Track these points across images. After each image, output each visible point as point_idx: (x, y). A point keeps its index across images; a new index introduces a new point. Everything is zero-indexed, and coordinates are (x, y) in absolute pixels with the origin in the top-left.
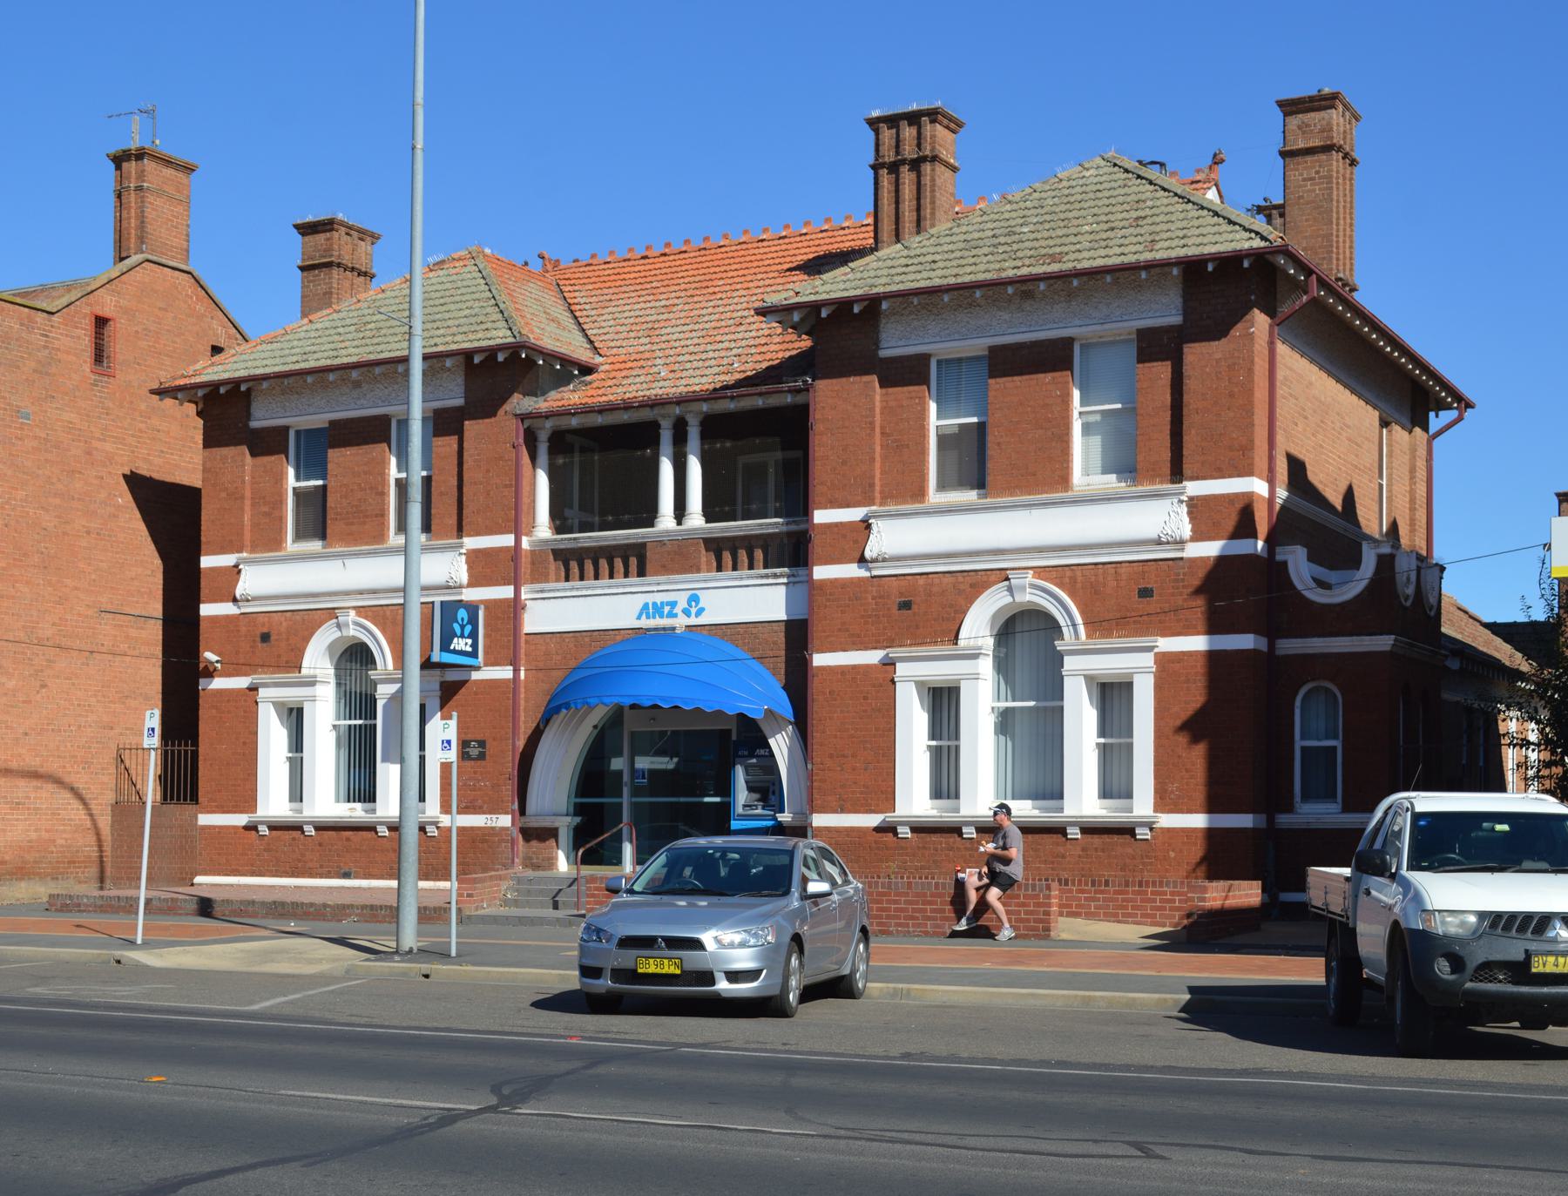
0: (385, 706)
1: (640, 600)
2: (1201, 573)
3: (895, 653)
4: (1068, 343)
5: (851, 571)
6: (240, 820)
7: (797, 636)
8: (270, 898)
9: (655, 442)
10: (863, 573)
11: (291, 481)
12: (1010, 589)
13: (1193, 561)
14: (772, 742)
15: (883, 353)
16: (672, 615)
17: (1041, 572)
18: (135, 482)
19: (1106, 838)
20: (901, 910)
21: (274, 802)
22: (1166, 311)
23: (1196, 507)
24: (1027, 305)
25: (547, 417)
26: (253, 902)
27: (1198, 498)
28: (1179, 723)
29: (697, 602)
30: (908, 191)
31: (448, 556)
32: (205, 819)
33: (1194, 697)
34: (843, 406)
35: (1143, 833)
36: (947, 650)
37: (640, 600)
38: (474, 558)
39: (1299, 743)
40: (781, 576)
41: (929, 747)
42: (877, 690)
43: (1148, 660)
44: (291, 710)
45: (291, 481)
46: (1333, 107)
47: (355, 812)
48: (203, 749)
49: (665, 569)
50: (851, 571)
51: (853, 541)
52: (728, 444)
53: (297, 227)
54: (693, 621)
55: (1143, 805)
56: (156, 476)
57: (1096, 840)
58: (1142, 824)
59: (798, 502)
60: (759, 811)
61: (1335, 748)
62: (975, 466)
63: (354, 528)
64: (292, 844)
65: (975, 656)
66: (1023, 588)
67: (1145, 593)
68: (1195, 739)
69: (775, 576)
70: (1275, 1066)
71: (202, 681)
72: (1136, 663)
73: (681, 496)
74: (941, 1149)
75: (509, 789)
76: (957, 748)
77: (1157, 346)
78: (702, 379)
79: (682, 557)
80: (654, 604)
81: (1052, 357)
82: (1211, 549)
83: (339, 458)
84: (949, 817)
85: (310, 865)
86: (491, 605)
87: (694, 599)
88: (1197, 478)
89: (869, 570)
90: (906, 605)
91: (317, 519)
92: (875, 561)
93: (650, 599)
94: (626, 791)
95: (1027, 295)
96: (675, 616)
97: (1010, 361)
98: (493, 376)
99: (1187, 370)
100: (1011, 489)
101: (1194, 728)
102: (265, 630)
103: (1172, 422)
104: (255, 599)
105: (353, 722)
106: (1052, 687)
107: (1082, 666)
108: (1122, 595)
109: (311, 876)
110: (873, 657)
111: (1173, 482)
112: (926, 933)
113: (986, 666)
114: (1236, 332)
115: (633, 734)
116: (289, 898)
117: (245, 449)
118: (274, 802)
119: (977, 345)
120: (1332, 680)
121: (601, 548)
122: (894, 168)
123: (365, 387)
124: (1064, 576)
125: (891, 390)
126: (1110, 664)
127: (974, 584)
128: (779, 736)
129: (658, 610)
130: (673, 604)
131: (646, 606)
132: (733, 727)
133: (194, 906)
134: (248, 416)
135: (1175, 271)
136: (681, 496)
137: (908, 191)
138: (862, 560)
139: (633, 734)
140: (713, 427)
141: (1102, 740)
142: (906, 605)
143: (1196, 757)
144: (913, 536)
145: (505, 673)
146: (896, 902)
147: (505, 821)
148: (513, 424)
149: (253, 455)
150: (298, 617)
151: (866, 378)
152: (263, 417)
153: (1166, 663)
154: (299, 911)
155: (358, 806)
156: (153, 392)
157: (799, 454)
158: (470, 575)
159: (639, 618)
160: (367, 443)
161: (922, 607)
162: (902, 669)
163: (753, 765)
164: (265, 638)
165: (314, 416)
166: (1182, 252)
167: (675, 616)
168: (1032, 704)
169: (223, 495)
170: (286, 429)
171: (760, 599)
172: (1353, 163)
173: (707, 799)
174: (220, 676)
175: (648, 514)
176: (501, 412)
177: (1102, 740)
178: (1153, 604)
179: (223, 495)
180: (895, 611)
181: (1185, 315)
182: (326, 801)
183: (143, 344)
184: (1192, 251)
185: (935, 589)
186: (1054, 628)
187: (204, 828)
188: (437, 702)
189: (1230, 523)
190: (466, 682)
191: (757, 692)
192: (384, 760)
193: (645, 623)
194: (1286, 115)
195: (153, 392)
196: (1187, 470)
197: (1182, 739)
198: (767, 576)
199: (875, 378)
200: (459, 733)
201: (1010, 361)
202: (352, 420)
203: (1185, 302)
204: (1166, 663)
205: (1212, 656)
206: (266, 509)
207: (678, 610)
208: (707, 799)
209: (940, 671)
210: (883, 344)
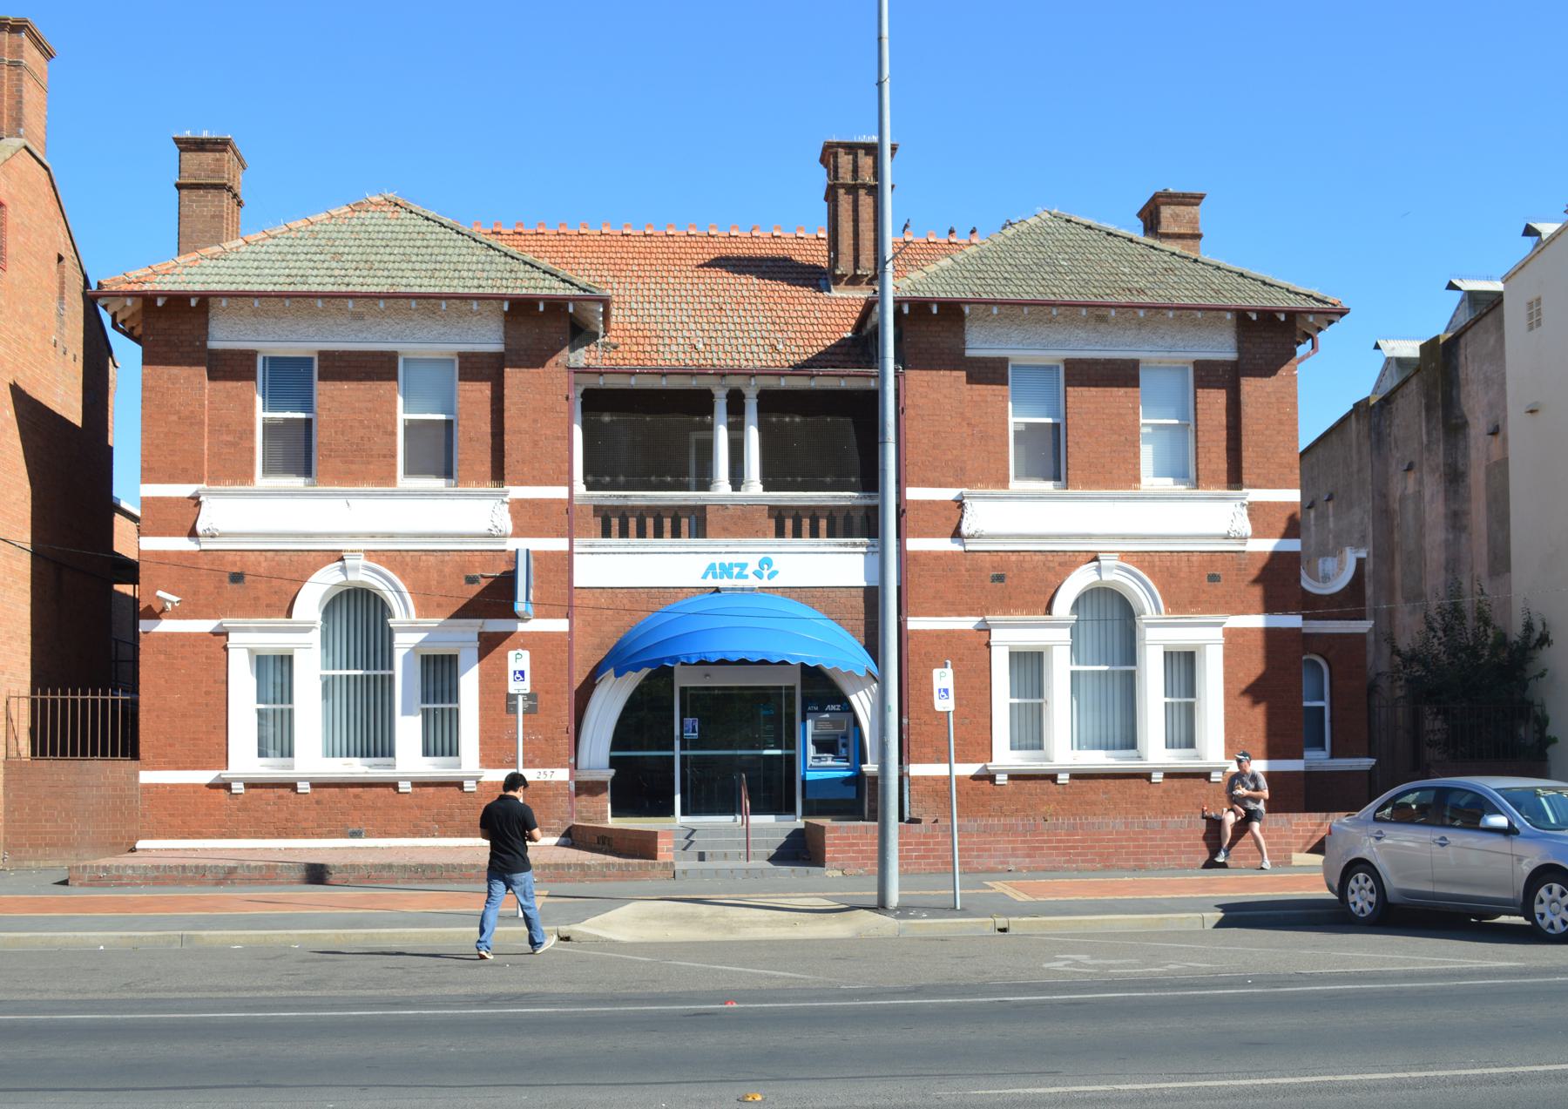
0: (405, 657)
1: (707, 560)
2: (1260, 564)
3: (228, 622)
4: (1004, 362)
5: (945, 545)
6: (205, 777)
7: (872, 597)
8: (405, 861)
9: (709, 410)
10: (956, 547)
11: (261, 414)
12: (1099, 569)
13: (1252, 554)
14: (853, 699)
15: (969, 353)
16: (741, 576)
18: (16, 391)
19: (1191, 781)
20: (1158, 846)
21: (245, 759)
22: (1222, 348)
23: (1254, 510)
24: (1102, 327)
25: (752, 375)
26: (390, 867)
27: (1256, 503)
28: (1243, 687)
29: (770, 564)
30: (866, 212)
31: (488, 504)
32: (147, 777)
33: (1255, 666)
34: (910, 398)
36: (281, 621)
37: (707, 560)
39: (1325, 704)
40: (861, 545)
42: (971, 657)
43: (1218, 633)
44: (259, 657)
45: (261, 414)
46: (225, 150)
47: (357, 768)
49: (726, 532)
50: (945, 545)
51: (951, 520)
52: (797, 419)
53: (177, 141)
54: (765, 583)
55: (1212, 751)
57: (1177, 783)
58: (1217, 769)
59: (870, 480)
60: (829, 763)
62: (1052, 458)
63: (354, 467)
64: (273, 804)
65: (307, 630)
66: (356, 569)
67: (1213, 578)
68: (1256, 702)
69: (855, 545)
70: (1476, 964)
71: (144, 625)
72: (1207, 637)
73: (737, 468)
75: (565, 743)
76: (291, 712)
77: (1206, 375)
78: (760, 358)
79: (740, 522)
80: (722, 565)
81: (1123, 375)
82: (1268, 545)
83: (330, 395)
84: (1045, 767)
85: (304, 825)
86: (542, 558)
87: (766, 562)
88: (1255, 487)
90: (1000, 578)
91: (297, 453)
92: (972, 537)
93: (717, 559)
94: (677, 744)
95: (1102, 319)
96: (746, 577)
97: (1082, 373)
98: (546, 324)
99: (1244, 398)
100: (1088, 484)
101: (1256, 692)
103: (1229, 439)
104: (222, 535)
105: (352, 672)
106: (1129, 652)
107: (1158, 639)
108: (1192, 579)
109: (305, 836)
110: (968, 623)
111: (1229, 488)
112: (1182, 867)
113: (315, 637)
114: (1283, 372)
115: (683, 690)
116: (427, 859)
117: (204, 370)
118: (245, 759)
119: (1056, 355)
121: (648, 508)
122: (853, 190)
124: (395, 560)
125: (160, 369)
126: (1182, 636)
127: (1067, 562)
128: (861, 693)
129: (726, 570)
130: (743, 566)
131: (712, 566)
132: (795, 680)
133: (302, 874)
134: (205, 335)
135: (1229, 316)
136: (737, 468)
137: (866, 212)
139: (683, 690)
140: (771, 402)
142: (1000, 578)
143: (1258, 715)
144: (1013, 515)
145: (561, 625)
146: (1152, 839)
147: (562, 775)
148: (563, 378)
149: (211, 378)
150: (284, 558)
151: (956, 373)
152: (223, 336)
153: (1232, 636)
154: (428, 874)
158: (515, 526)
159: (705, 577)
160: (371, 379)
161: (1021, 580)
162: (997, 635)
163: (826, 720)
164: (237, 578)
165: (302, 342)
167: (746, 577)
168: (1106, 668)
169: (175, 418)
171: (839, 565)
172: (240, 204)
173: (767, 752)
174: (171, 617)
176: (551, 363)
178: (1220, 588)
179: (175, 418)
180: (988, 583)
181: (1239, 350)
182: (314, 756)
184: (1267, 304)
185: (1026, 565)
186: (383, 608)
187: (147, 787)
188: (475, 653)
189: (1282, 526)
190: (511, 633)
191: (839, 651)
192: (404, 714)
193: (711, 582)
194: (182, 150)
196: (1246, 479)
197: (1246, 701)
198: (846, 545)
199: (964, 373)
200: (955, 683)
201: (1082, 373)
202: (350, 353)
203: (506, 333)
204: (1232, 636)
205: (1269, 633)
206: (230, 438)
207: (749, 571)
208: (767, 752)
209: (1028, 638)
210: (969, 345)
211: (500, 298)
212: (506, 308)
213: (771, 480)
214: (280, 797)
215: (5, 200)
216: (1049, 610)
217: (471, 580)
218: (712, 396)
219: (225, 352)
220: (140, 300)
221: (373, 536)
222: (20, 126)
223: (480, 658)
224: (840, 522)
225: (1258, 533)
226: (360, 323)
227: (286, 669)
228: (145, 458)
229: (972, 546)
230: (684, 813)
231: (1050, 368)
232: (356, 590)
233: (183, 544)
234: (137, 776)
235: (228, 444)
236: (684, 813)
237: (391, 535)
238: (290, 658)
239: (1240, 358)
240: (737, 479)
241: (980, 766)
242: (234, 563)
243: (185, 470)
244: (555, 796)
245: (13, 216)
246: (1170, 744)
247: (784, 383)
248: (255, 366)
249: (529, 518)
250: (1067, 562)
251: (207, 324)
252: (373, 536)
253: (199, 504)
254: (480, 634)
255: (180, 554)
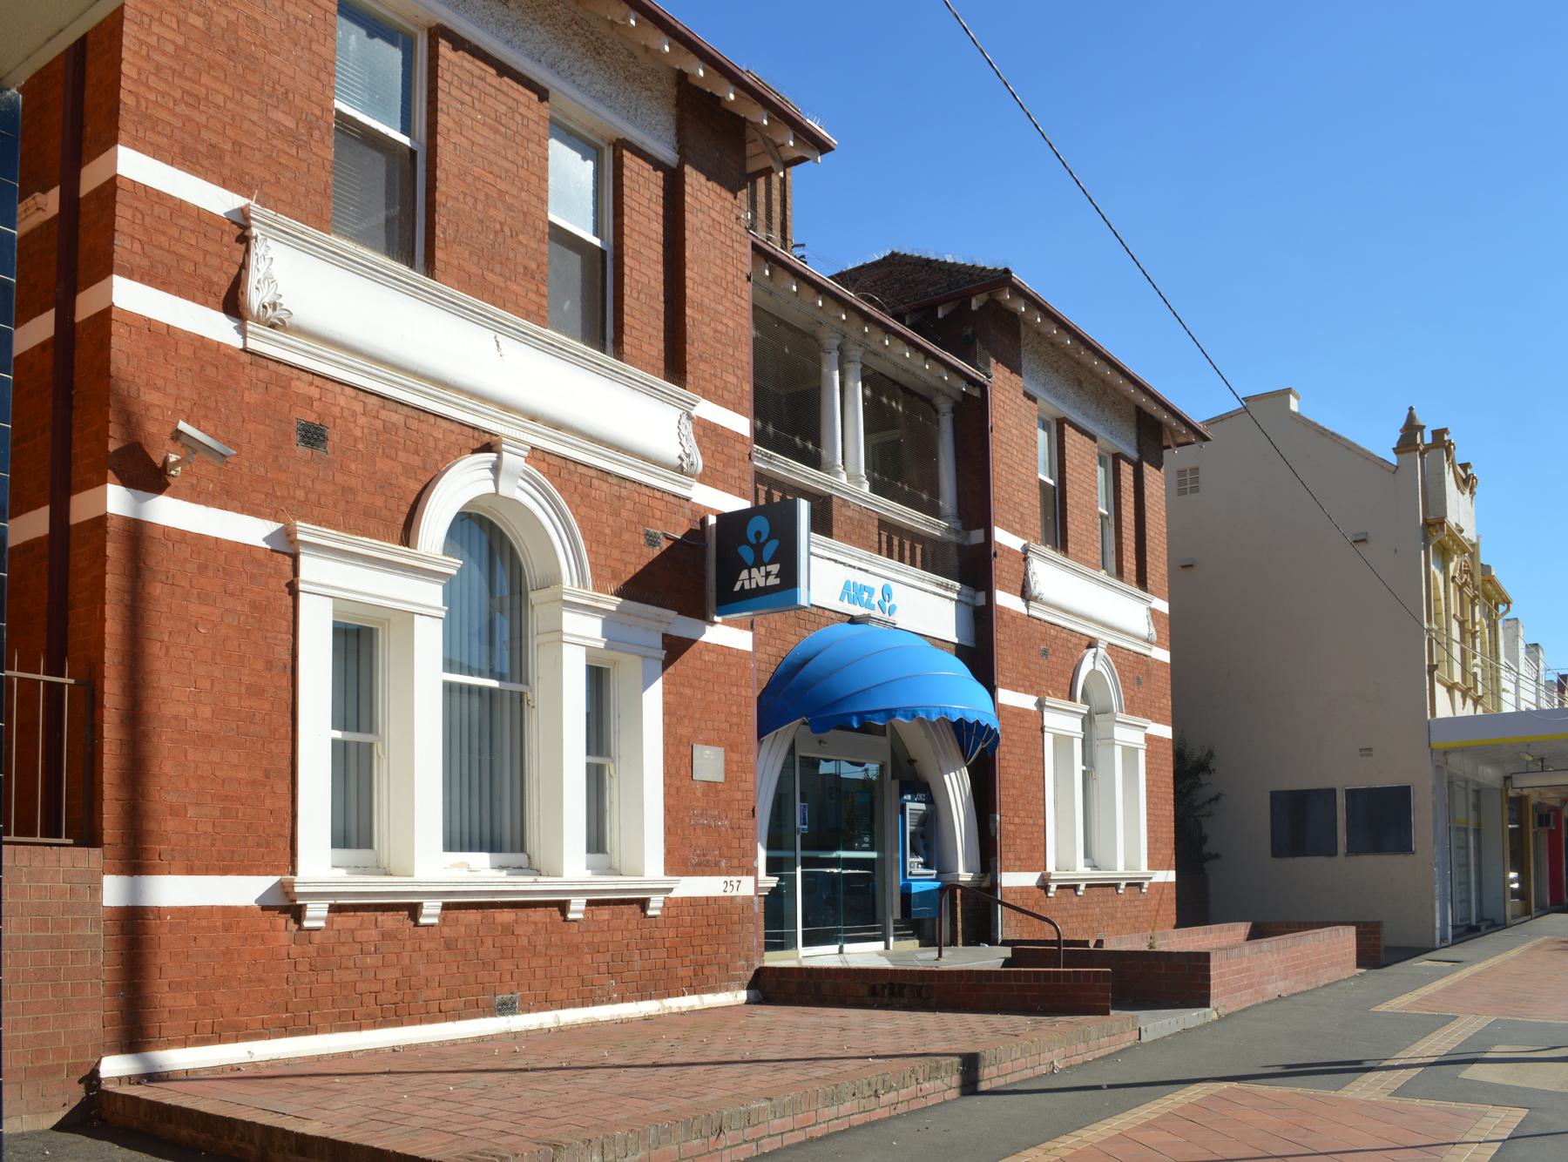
3: (305, 531)
6: (243, 890)
12: (496, 469)
17: (537, 456)
35: (656, 906)
41: (334, 742)
47: (479, 872)
55: (647, 864)
56: (994, 437)
57: (604, 913)
69: (947, 588)
74: (1225, 1085)
89: (242, 331)
138: (233, 305)
141: (338, 735)
155: (481, 860)
162: (311, 568)
164: (313, 435)
177: (338, 735)
214: (386, 936)
216: (407, 535)
217: (652, 540)
221: (534, 418)
223: (664, 668)
225: (708, 477)
229: (263, 343)
230: (805, 944)
233: (215, 326)
235: (283, 133)
236: (805, 944)
237: (558, 426)
241: (271, 881)
243: (215, 153)
244: (741, 922)
246: (455, 842)
252: (534, 418)
253: (244, 239)
255: (201, 343)
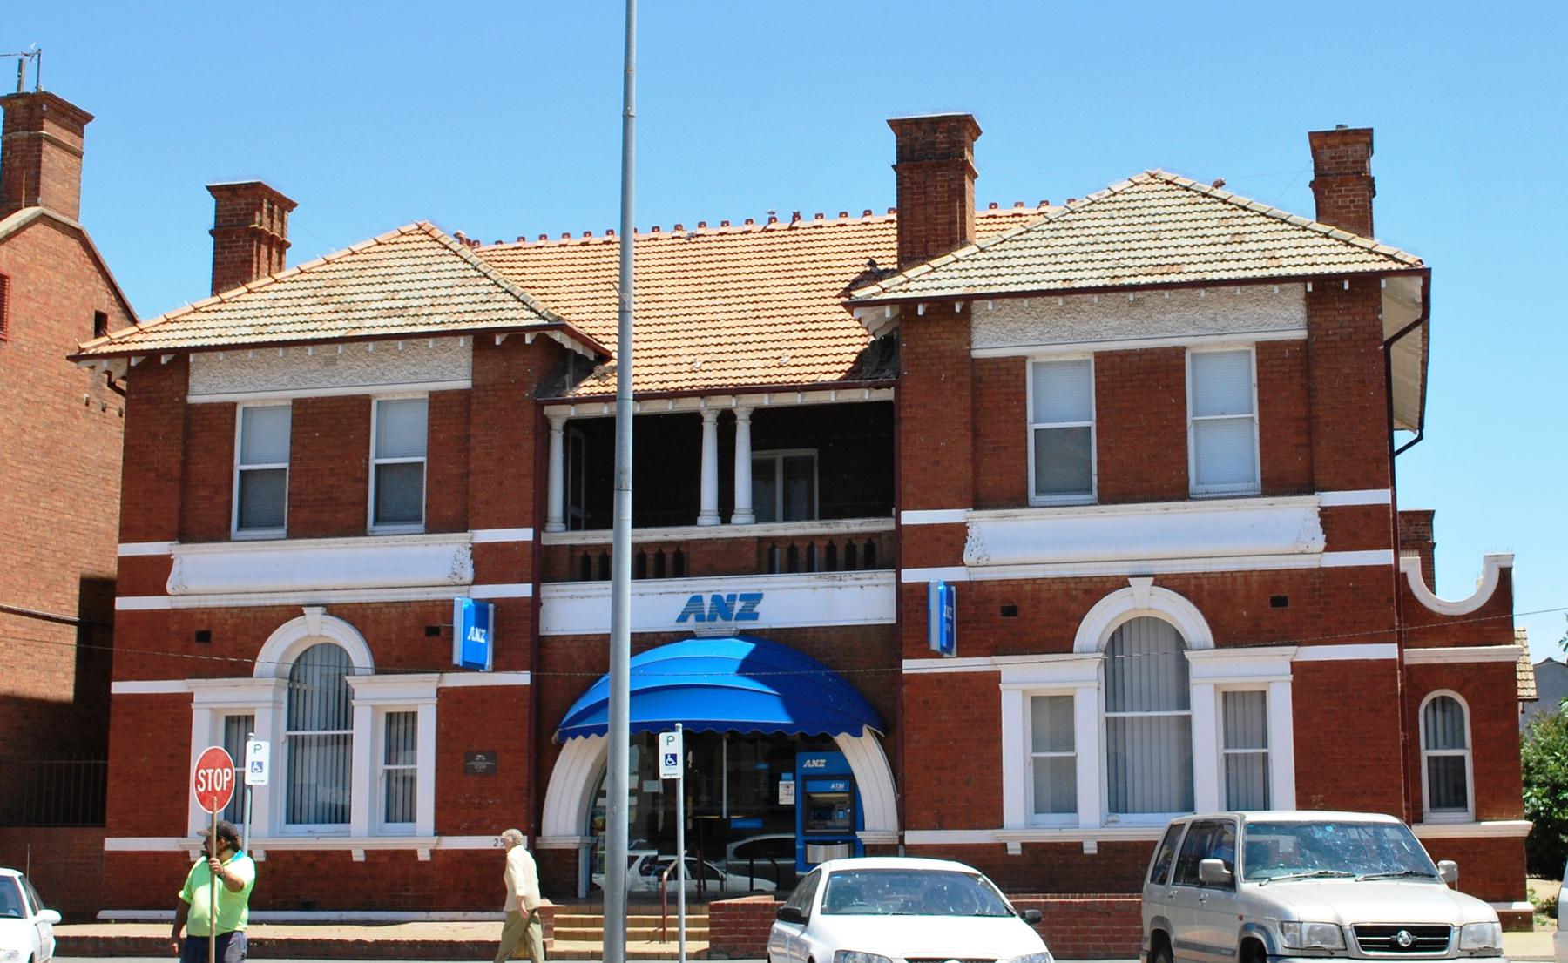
32: (112, 844)
38: (1328, 517)
39: (1467, 753)
44: (1225, 694)
48: (112, 763)
51: (949, 546)
61: (1462, 758)
67: (1279, 602)
102: (203, 628)
120: (1460, 690)
123: (341, 364)
124: (1186, 586)
127: (1095, 589)
156: (70, 358)
157: (362, 485)
164: (204, 637)
166: (1316, 270)
169: (152, 475)
170: (234, 405)
175: (690, 515)
179: (152, 475)
183: (33, 305)
195: (70, 358)
203: (1309, 317)
211: (1303, 279)
212: (1310, 288)
213: (762, 512)
215: (5, 272)
218: (734, 417)
219: (204, 405)
220: (897, 308)
222: (38, 194)
224: (651, 563)
226: (333, 368)
227: (410, 725)
228: (125, 516)
231: (1079, 363)
232: (329, 645)
234: (103, 844)
238: (414, 715)
239: (1310, 336)
240: (726, 510)
242: (202, 621)
245: (15, 289)
247: (831, 397)
248: (234, 418)
249: (489, 564)
250: (1095, 589)
251: (970, 333)
254: (439, 690)
